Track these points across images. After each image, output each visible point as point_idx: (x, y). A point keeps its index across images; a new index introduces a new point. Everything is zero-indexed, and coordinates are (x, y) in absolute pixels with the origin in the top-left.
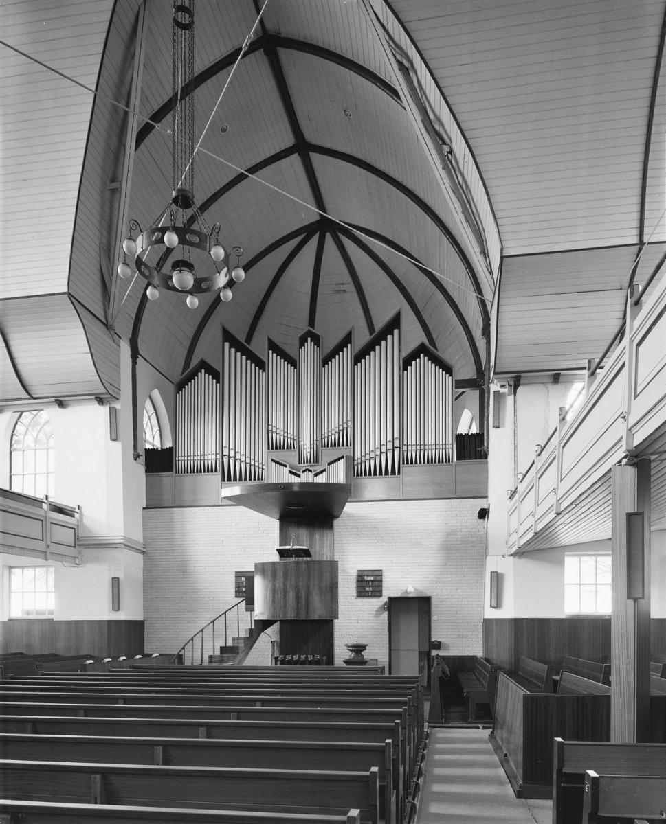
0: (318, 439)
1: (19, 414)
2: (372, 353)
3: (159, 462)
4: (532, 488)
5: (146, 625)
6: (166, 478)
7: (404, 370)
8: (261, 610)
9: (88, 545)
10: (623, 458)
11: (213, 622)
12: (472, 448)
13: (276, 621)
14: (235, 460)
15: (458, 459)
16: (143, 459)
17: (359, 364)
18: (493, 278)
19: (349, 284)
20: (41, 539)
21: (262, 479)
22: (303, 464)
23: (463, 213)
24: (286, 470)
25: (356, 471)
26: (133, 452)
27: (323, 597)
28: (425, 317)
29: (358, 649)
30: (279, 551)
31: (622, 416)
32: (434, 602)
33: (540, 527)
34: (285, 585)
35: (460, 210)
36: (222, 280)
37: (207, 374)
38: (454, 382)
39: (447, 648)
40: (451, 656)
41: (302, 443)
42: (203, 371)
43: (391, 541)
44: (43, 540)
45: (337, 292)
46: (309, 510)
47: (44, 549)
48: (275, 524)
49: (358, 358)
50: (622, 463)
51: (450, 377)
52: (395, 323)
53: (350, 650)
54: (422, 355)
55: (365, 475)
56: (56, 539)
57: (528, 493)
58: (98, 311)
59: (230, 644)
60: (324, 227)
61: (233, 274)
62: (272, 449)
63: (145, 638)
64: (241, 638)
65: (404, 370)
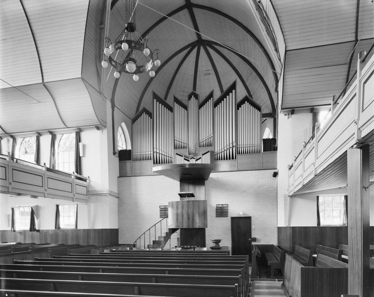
0: (198, 143)
1: (62, 135)
2: (222, 102)
3: (125, 156)
4: (292, 174)
5: (119, 231)
6: (128, 164)
7: (237, 110)
8: (170, 222)
9: (93, 194)
10: (354, 145)
11: (149, 229)
12: (270, 145)
13: (179, 229)
14: (159, 154)
15: (264, 151)
16: (117, 155)
17: (216, 107)
18: (281, 62)
19: (212, 70)
20: (5, 179)
21: (172, 163)
22: (191, 155)
23: (266, 31)
24: (183, 158)
25: (215, 158)
26: (113, 151)
27: (200, 217)
28: (248, 84)
29: (217, 242)
30: (180, 195)
31: (354, 122)
32: (253, 219)
33: (306, 182)
34: (182, 212)
35: (264, 29)
36: (149, 66)
37: (146, 115)
38: (261, 115)
39: (259, 241)
40: (261, 245)
41: (190, 145)
42: (144, 113)
43: (233, 192)
44: (42, 187)
45: (206, 74)
46: (193, 176)
47: (13, 183)
48: (178, 183)
49: (216, 104)
50: (354, 147)
51: (260, 112)
52: (233, 87)
53: (213, 242)
54: (246, 102)
55: (220, 160)
56: (78, 192)
57: (299, 166)
58: (97, 88)
59: (157, 239)
60: (200, 43)
61: (155, 62)
62: (176, 148)
63: (119, 237)
64: (162, 237)
65: (237, 110)
